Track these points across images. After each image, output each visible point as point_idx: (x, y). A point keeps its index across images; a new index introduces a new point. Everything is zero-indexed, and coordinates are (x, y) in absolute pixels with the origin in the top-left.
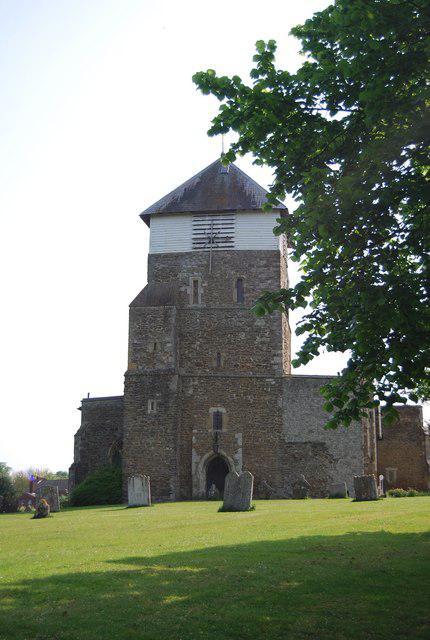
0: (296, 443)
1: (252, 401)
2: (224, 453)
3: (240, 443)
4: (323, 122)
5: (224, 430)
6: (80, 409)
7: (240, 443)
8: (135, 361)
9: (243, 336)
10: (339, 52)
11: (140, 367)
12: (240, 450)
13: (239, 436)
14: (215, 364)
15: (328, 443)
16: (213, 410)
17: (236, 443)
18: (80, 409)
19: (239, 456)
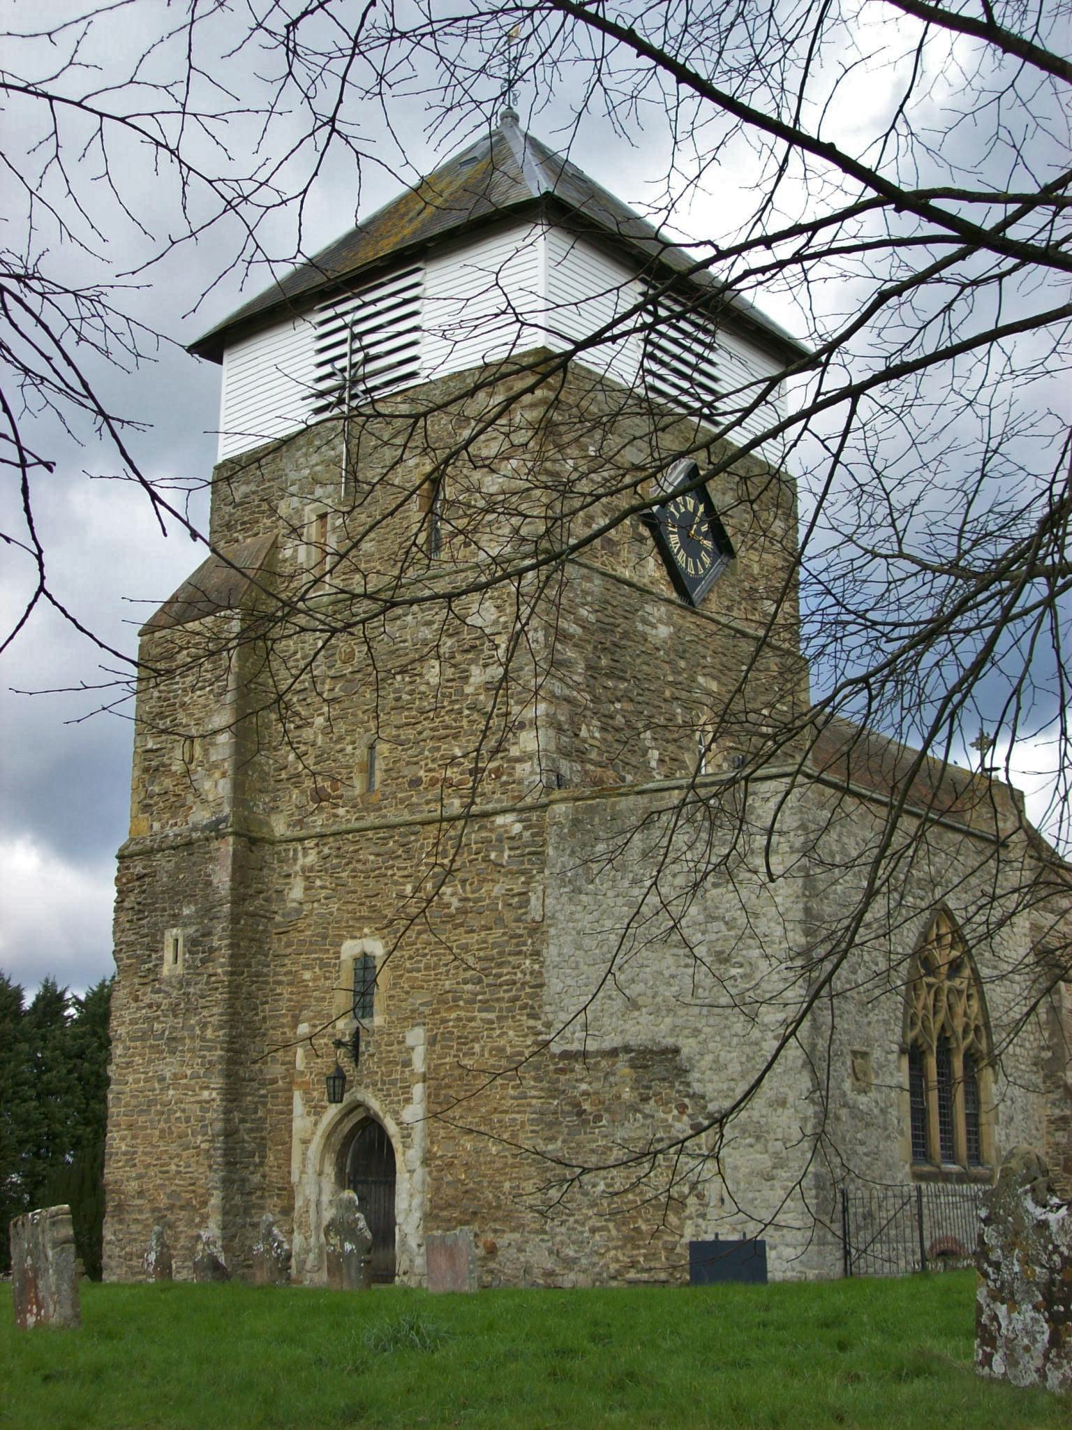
0: (585, 1054)
1: (455, 903)
2: (375, 1105)
3: (419, 1065)
4: (366, 1218)
5: (378, 1020)
6: (638, 56)
7: (419, 1065)
8: (146, 808)
9: (433, 673)
10: (583, 612)
11: (156, 826)
12: (418, 1090)
13: (416, 1037)
14: (358, 784)
15: (688, 1046)
16: (350, 949)
17: (407, 1063)
18: (638, 56)
19: (414, 1112)
